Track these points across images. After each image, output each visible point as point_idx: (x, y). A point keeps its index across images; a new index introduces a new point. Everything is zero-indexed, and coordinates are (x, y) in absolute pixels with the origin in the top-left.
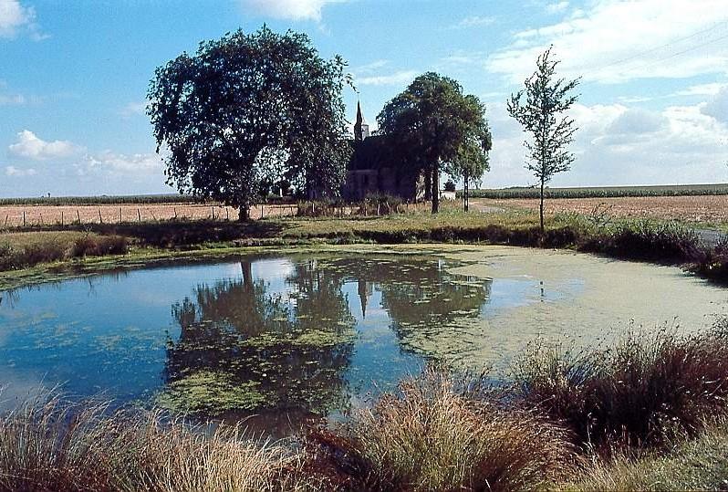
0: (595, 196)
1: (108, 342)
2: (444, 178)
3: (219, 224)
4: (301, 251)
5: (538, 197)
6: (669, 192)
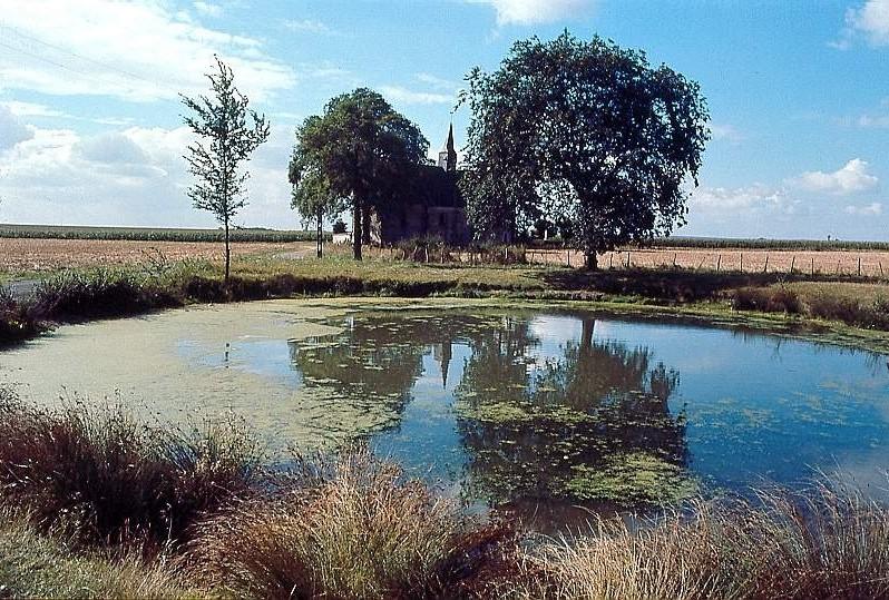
0: (162, 240)
1: (757, 418)
2: (655, 108)
3: (621, 274)
4: (522, 306)
5: (219, 240)
6: (72, 234)
